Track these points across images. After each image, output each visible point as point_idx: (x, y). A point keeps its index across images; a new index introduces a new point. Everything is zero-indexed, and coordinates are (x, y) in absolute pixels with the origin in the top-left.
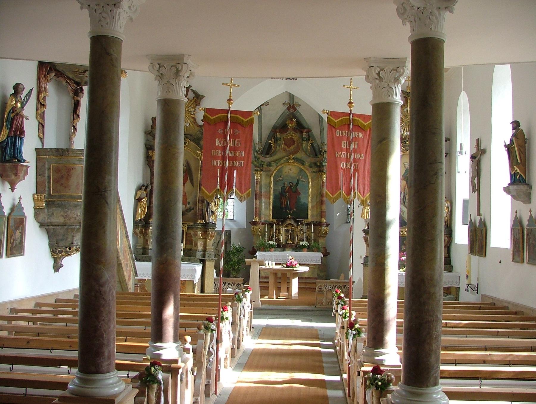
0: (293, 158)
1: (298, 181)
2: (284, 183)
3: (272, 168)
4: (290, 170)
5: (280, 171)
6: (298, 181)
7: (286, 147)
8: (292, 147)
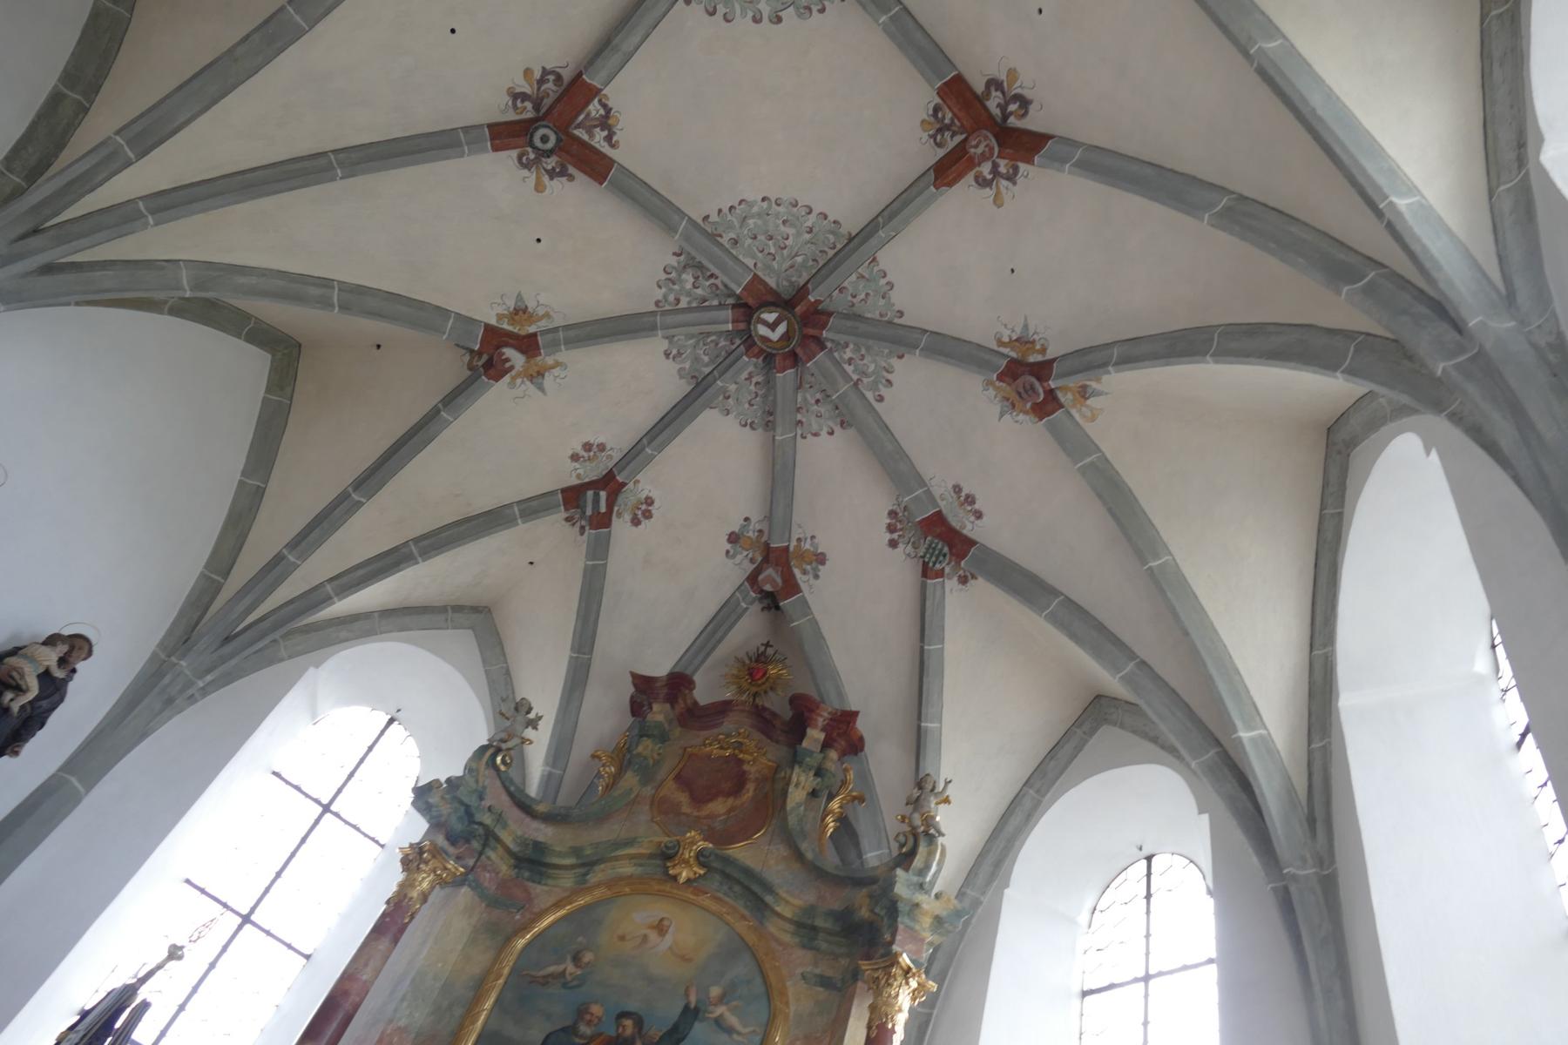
0: (700, 854)
1: (691, 1014)
2: (582, 1012)
3: (542, 893)
4: (661, 928)
5: (585, 921)
6: (691, 1014)
7: (683, 798)
8: (719, 807)
